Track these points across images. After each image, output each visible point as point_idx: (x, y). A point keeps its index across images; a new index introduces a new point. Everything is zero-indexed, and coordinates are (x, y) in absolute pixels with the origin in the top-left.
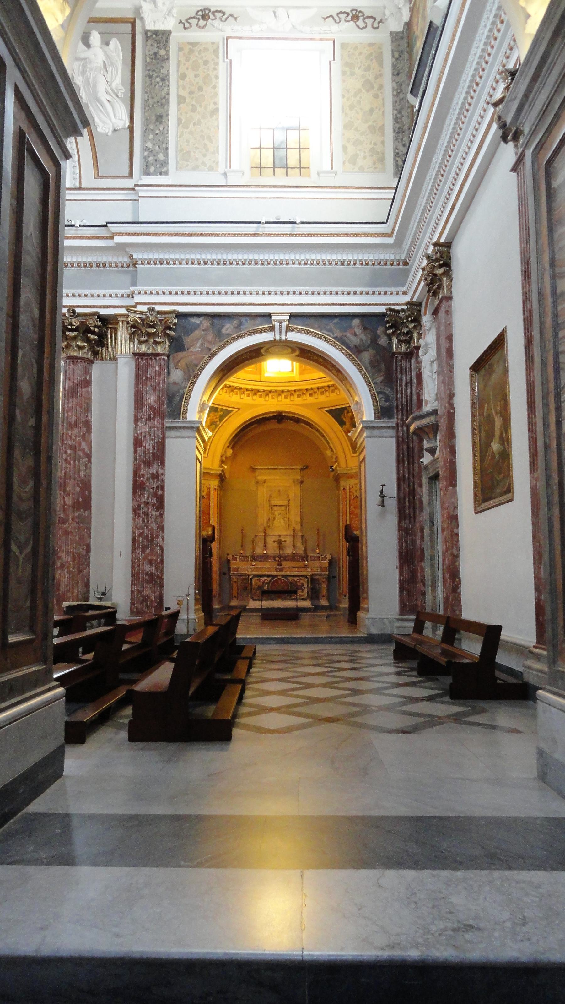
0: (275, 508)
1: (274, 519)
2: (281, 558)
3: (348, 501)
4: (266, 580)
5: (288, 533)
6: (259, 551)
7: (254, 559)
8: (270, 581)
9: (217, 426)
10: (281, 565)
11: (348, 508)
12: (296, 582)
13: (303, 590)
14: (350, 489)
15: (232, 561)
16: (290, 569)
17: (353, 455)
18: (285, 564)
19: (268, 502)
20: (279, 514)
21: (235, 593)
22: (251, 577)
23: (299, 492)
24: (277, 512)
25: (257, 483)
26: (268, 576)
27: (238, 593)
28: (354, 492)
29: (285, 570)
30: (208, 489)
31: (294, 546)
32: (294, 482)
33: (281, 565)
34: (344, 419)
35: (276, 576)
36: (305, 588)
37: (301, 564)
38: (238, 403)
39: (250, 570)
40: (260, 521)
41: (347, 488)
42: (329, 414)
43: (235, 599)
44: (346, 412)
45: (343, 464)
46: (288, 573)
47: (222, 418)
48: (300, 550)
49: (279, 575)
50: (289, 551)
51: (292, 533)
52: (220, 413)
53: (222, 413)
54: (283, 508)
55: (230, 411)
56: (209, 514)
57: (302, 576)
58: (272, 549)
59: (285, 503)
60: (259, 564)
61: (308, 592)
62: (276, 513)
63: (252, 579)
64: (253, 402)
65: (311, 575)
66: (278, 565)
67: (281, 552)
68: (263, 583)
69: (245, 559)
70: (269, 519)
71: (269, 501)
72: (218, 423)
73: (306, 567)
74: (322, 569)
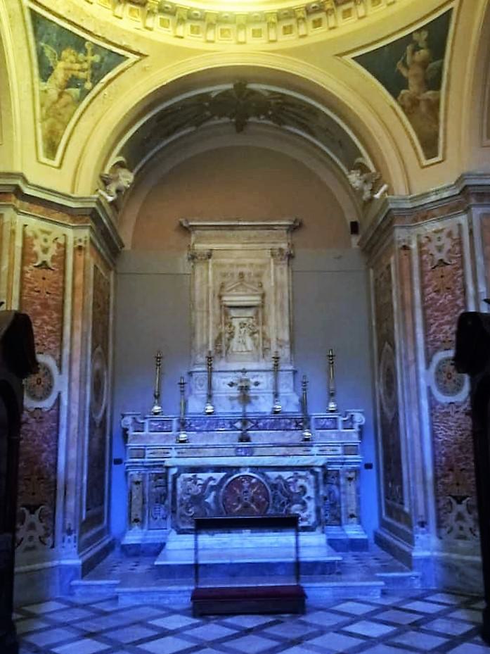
0: (233, 313)
1: (232, 335)
2: (246, 426)
3: (416, 279)
4: (211, 479)
5: (263, 365)
6: (196, 405)
7: (183, 425)
8: (223, 480)
9: (85, 93)
10: (248, 440)
11: (417, 293)
12: (287, 484)
13: (304, 504)
14: (420, 245)
15: (131, 433)
16: (269, 453)
17: (425, 162)
18: (259, 437)
19: (217, 301)
20: (242, 325)
21: (136, 512)
22: (174, 471)
23: (284, 277)
24: (237, 319)
25: (193, 258)
26: (218, 469)
27: (143, 510)
28: (435, 252)
29: (258, 451)
30: (59, 245)
31: (276, 395)
32: (273, 255)
33: (248, 440)
34: (404, 73)
35: (238, 468)
36: (309, 498)
37: (295, 436)
38: (138, 39)
39: (174, 453)
40: (199, 341)
41: (414, 246)
42: (364, 71)
43: (136, 527)
44: (409, 48)
45: (400, 190)
46: (267, 461)
47: (97, 72)
48: (289, 404)
49: (245, 467)
50: (264, 405)
51: (270, 365)
52: (90, 58)
53: (97, 58)
54: (250, 313)
55: (122, 58)
56: (61, 310)
57: (302, 468)
58: (226, 405)
59: (255, 300)
60: (197, 439)
61: (318, 511)
62: (236, 323)
63: (175, 477)
64: (178, 42)
65: (323, 467)
66: (241, 440)
67: (249, 409)
68: (204, 486)
69: (163, 426)
70: (220, 336)
71: (220, 297)
72: (88, 85)
73: (307, 443)
74: (348, 449)
